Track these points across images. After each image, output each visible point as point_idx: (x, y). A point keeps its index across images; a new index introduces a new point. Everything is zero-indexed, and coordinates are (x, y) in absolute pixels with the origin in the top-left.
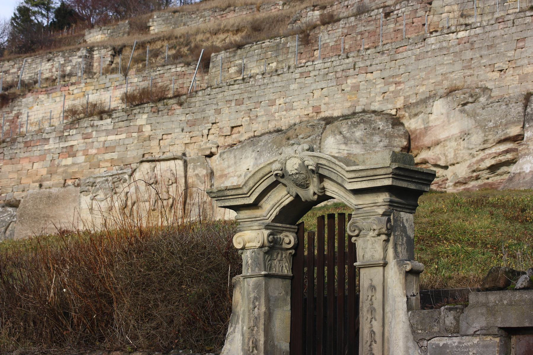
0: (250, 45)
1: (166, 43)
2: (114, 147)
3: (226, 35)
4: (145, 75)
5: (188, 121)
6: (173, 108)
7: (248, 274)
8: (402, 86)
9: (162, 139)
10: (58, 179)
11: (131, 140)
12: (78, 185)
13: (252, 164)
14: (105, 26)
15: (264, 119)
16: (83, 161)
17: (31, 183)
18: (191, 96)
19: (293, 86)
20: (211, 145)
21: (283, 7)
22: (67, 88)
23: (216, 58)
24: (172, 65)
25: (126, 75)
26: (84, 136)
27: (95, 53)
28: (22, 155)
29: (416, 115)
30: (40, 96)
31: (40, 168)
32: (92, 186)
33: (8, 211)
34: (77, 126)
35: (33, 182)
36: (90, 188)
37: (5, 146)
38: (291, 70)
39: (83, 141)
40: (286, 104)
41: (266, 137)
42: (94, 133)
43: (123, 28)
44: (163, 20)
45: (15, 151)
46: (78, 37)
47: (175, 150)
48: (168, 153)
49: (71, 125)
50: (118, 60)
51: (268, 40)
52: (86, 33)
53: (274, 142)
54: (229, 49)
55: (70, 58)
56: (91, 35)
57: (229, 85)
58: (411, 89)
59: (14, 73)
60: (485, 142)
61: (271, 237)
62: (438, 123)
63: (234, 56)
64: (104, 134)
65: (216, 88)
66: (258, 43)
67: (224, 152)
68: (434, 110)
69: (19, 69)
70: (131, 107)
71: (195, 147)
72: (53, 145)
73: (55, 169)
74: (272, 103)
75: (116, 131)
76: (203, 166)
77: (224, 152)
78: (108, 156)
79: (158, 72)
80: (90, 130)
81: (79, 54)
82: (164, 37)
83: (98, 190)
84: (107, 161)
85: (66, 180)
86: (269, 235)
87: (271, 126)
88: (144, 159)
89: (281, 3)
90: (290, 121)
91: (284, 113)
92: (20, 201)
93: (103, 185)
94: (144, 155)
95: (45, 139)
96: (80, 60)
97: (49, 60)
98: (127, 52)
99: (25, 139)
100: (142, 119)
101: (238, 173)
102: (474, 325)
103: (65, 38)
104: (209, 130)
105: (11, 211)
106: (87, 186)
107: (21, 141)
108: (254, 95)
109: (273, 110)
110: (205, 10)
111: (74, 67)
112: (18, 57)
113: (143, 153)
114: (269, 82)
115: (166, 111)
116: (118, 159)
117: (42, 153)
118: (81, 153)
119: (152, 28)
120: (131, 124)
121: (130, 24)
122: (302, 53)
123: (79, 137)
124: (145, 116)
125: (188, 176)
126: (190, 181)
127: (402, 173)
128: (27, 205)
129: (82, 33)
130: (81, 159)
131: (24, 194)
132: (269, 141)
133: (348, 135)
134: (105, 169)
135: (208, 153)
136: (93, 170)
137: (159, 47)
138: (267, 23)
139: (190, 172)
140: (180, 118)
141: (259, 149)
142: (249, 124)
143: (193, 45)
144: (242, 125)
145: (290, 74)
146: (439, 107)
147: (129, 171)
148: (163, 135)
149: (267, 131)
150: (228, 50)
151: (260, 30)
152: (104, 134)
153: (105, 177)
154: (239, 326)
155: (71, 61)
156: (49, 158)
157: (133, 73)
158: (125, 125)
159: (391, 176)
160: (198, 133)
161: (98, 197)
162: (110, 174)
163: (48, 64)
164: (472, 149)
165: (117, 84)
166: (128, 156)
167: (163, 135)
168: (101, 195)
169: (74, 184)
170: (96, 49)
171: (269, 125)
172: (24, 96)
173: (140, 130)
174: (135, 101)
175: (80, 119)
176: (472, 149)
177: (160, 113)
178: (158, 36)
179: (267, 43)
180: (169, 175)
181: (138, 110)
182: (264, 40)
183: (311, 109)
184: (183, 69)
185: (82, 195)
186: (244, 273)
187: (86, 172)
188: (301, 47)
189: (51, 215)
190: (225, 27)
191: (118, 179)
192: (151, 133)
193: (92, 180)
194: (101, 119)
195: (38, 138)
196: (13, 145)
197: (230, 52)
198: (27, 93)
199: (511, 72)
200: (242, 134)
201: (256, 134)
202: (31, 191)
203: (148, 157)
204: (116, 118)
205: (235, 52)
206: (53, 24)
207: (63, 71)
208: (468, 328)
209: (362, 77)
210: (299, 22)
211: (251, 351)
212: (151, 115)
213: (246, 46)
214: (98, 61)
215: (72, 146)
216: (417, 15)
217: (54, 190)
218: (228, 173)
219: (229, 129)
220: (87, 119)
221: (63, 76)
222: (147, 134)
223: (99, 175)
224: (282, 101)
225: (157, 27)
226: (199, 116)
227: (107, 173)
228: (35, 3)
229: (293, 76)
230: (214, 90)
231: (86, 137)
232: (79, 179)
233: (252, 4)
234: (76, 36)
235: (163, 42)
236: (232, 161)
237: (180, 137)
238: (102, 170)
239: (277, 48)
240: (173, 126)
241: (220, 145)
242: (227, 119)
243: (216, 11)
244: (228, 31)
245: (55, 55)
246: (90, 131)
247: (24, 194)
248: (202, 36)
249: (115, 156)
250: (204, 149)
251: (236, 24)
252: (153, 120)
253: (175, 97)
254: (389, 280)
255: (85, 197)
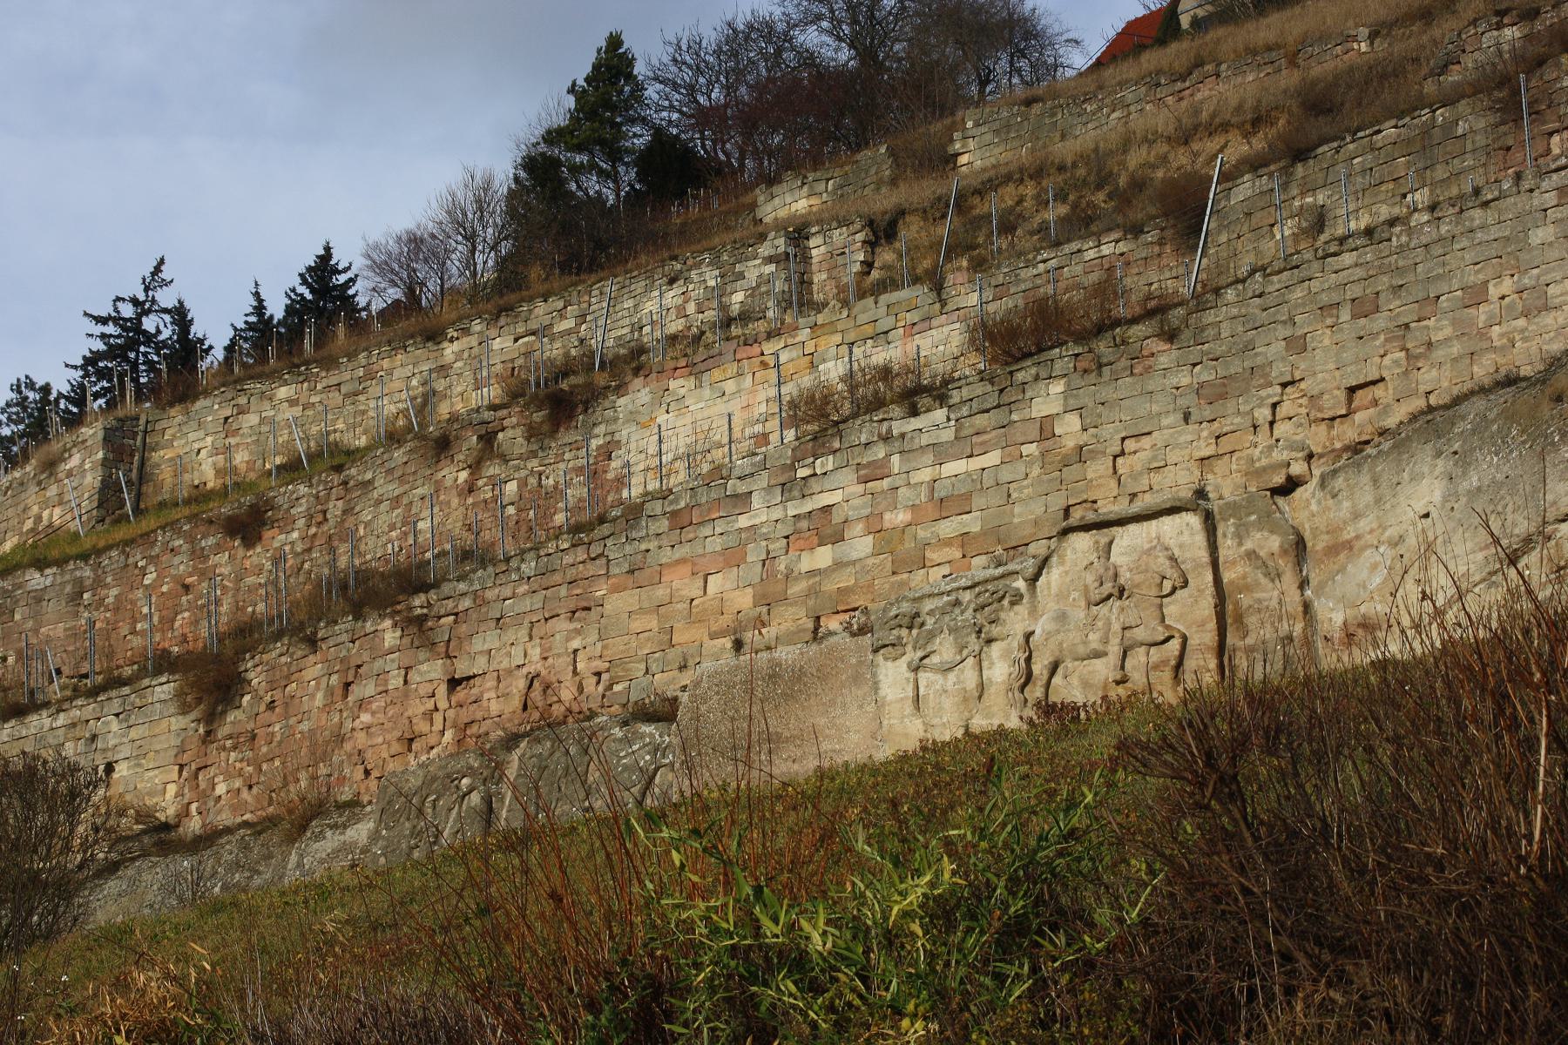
0: (1335, 144)
1: (1029, 190)
2: (968, 496)
3: (1223, 141)
4: (1000, 279)
5: (1201, 385)
6: (1145, 353)
9: (1123, 453)
10: (789, 619)
11: (1021, 468)
12: (863, 630)
13: (1437, 496)
14: (815, 170)
15: (1456, 349)
16: (869, 550)
17: (706, 638)
18: (1201, 308)
19: (1539, 236)
20: (1285, 456)
21: (1372, 43)
22: (756, 349)
23: (1228, 198)
24: (1083, 238)
25: (938, 288)
26: (862, 472)
27: (812, 243)
28: (667, 556)
30: (673, 384)
31: (731, 591)
32: (910, 628)
33: (643, 736)
34: (836, 445)
36: (904, 632)
37: (607, 533)
38: (1526, 185)
39: (860, 488)
40: (1525, 295)
41: (1479, 403)
42: (896, 459)
43: (873, 171)
44: (996, 132)
45: (643, 547)
46: (736, 213)
47: (1168, 482)
48: (1147, 496)
49: (816, 444)
50: (886, 256)
51: (1393, 122)
52: (761, 199)
53: (1509, 416)
54: (1266, 165)
55: (738, 268)
56: (777, 201)
57: (1324, 258)
59: (569, 332)
63: (1285, 186)
64: (929, 458)
65: (1280, 272)
66: (1360, 134)
67: (1335, 472)
69: (582, 318)
70: (1007, 364)
71: (1234, 467)
72: (763, 512)
73: (780, 587)
74: (1476, 295)
75: (965, 445)
76: (1269, 522)
77: (1335, 472)
79: (1041, 267)
80: (880, 452)
81: (765, 250)
82: (1021, 170)
83: (932, 635)
84: (948, 542)
85: (818, 618)
87: (1482, 370)
89: (1364, 32)
90: (1545, 347)
91: (1522, 322)
92: (676, 699)
93: (947, 618)
94: (1067, 511)
95: (736, 496)
97: (672, 281)
98: (911, 230)
99: (671, 503)
100: (1048, 399)
101: (1391, 532)
103: (694, 222)
104: (1274, 406)
105: (651, 735)
106: (890, 628)
107: (658, 511)
108: (1411, 277)
109: (1482, 318)
110: (1122, 84)
111: (753, 291)
112: (575, 284)
113: (1062, 503)
114: (1458, 230)
115: (1124, 363)
116: (984, 533)
117: (731, 541)
118: (859, 528)
119: (963, 159)
120: (1015, 417)
121: (892, 152)
122: (1509, 149)
123: (847, 476)
124: (1057, 387)
125: (1221, 560)
126: (1227, 576)
128: (703, 708)
129: (747, 199)
130: (860, 545)
131: (686, 678)
132: (1491, 416)
134: (946, 570)
135: (1279, 479)
136: (905, 576)
137: (1010, 203)
138: (1350, 87)
139: (1227, 548)
140: (1174, 381)
141: (1456, 446)
142: (1406, 373)
143: (1123, 181)
144: (1382, 379)
145: (1524, 197)
147: (1030, 566)
148: (1123, 439)
149: (1468, 386)
150: (1265, 170)
151: (1330, 111)
152: (929, 458)
153: (949, 593)
155: (741, 276)
156: (754, 554)
157: (960, 280)
158: (993, 424)
160: (1238, 420)
161: (935, 659)
162: (963, 582)
163: (671, 293)
165: (912, 317)
166: (1016, 520)
167: (1123, 439)
168: (944, 650)
169: (848, 627)
170: (813, 230)
171: (1475, 369)
172: (621, 389)
173: (1047, 434)
174: (1014, 344)
175: (844, 421)
177: (1106, 370)
178: (1004, 170)
179: (1389, 132)
180: (1162, 563)
181: (1033, 371)
182: (1379, 122)
184: (1122, 247)
185: (880, 658)
187: (883, 584)
188: (1503, 128)
189: (786, 734)
190: (1213, 116)
191: (994, 598)
192: (1085, 438)
193: (906, 607)
194: (914, 413)
195: (714, 495)
196: (632, 527)
197: (1271, 175)
198: (628, 378)
200: (1388, 405)
201: (1433, 400)
202: (708, 665)
203: (1077, 516)
204: (963, 402)
205: (1287, 172)
206: (634, 198)
207: (724, 308)
210: (1456, 67)
212: (1077, 380)
213: (1320, 150)
214: (825, 266)
215: (827, 509)
217: (785, 654)
218: (1358, 537)
219: (1342, 395)
220: (867, 417)
221: (727, 322)
222: (1070, 443)
223: (927, 590)
224: (1507, 286)
225: (975, 153)
226: (1236, 367)
227: (954, 580)
228: (575, 141)
229: (1536, 202)
230: (1275, 278)
231: (871, 474)
232: (866, 611)
233: (1269, 49)
234: (727, 213)
235: (1021, 188)
236: (1366, 497)
237: (1182, 439)
238: (936, 574)
239: (1424, 146)
240: (1155, 408)
241: (1317, 449)
242: (1332, 366)
243: (1158, 85)
244: (1225, 127)
245: (690, 262)
246: (881, 455)
247: (686, 678)
248: (1144, 150)
249: (972, 523)
250: (1264, 469)
251: (1250, 103)
252: (1086, 397)
253: (1149, 314)
255: (889, 664)
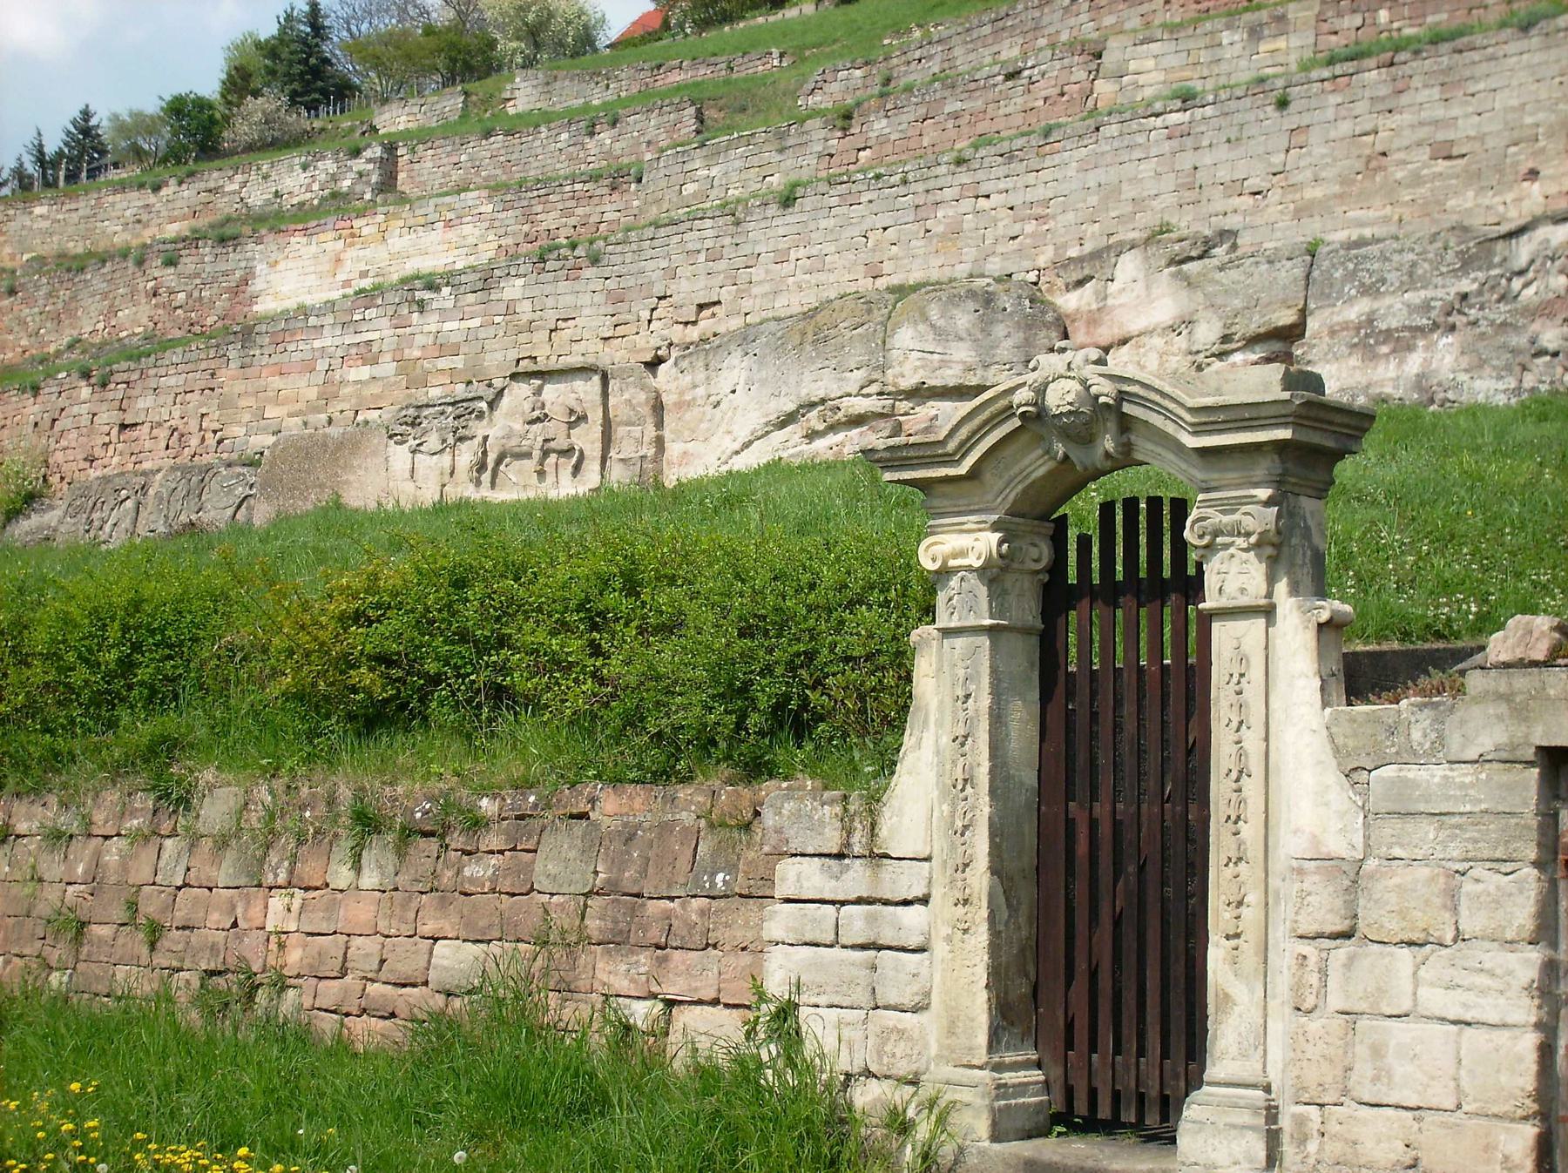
7: (952, 625)
8: (1051, 224)
11: (491, 331)
15: (767, 288)
29: (1080, 283)
34: (379, 302)
35: (290, 415)
58: (1073, 233)
59: (234, 192)
60: (1226, 339)
61: (1006, 546)
62: (1123, 299)
68: (1119, 274)
78: (443, 363)
86: (1000, 544)
88: (520, 369)
96: (371, 166)
102: (1481, 739)
118: (388, 357)
123: (385, 322)
127: (1313, 413)
130: (387, 368)
133: (941, 323)
146: (1128, 267)
154: (929, 739)
156: (322, 365)
159: (1290, 419)
164: (1198, 352)
168: (433, 442)
176: (1198, 352)
183: (862, 268)
186: (943, 620)
199: (1277, 197)
203: (526, 365)
208: (1463, 747)
209: (967, 204)
211: (960, 787)
216: (1073, 79)
219: (694, 308)
222: (525, 318)
224: (802, 253)
241: (675, 341)
249: (458, 362)
254: (1278, 641)
